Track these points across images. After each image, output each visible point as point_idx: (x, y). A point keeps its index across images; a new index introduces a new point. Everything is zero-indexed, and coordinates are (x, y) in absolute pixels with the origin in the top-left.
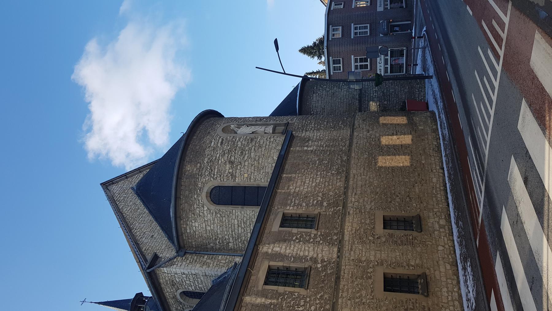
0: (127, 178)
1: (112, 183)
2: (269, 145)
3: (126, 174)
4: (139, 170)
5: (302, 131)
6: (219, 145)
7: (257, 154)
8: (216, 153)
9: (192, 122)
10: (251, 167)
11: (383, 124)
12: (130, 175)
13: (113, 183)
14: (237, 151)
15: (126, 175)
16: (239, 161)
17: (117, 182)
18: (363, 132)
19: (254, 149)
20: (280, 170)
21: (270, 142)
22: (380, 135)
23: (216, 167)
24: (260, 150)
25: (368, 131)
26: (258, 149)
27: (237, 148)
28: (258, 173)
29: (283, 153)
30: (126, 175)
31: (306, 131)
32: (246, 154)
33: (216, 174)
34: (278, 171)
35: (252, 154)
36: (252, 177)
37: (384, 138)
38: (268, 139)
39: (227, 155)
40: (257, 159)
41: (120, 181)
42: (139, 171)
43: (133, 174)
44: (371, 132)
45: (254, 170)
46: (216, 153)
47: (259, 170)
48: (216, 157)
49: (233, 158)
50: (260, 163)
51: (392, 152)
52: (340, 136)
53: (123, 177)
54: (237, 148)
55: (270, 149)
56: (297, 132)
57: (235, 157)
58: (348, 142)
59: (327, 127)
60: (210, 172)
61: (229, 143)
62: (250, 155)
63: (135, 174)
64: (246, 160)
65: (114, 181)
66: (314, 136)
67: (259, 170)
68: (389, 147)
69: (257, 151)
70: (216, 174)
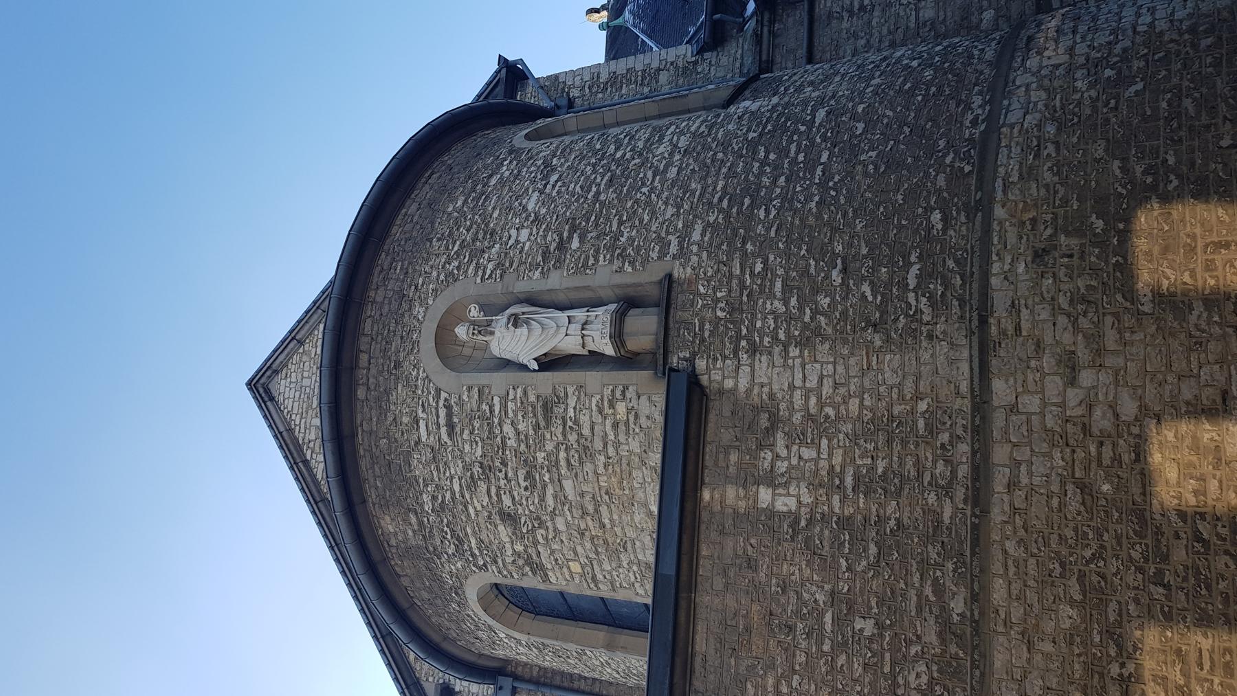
0: (301, 343)
1: (273, 373)
2: (617, 444)
3: (293, 335)
4: (318, 308)
5: (736, 352)
6: (445, 437)
7: (585, 489)
8: (448, 474)
9: (349, 234)
10: (582, 539)
11: (1163, 299)
12: (302, 332)
13: (276, 372)
14: (512, 468)
15: (295, 336)
16: (531, 512)
17: (285, 365)
18: (1043, 376)
19: (568, 461)
20: (675, 681)
21: (615, 425)
22: (1144, 411)
23: (469, 530)
24: (588, 467)
25: (1070, 369)
26: (581, 463)
27: (508, 452)
28: (614, 565)
29: (670, 570)
30: (293, 338)
31: (754, 350)
32: (544, 486)
33: (477, 552)
34: (667, 686)
35: (568, 485)
36: (599, 576)
37: (1170, 436)
38: (607, 411)
39: (483, 487)
40: (591, 509)
41: (289, 360)
42: (320, 311)
43: (311, 326)
44: (1086, 378)
45: (597, 553)
46: (448, 474)
47: (614, 554)
48: (453, 492)
49: (507, 501)
50: (608, 526)
51: (1222, 585)
52: (918, 396)
53: (291, 345)
54: (508, 452)
55: (624, 461)
56: (715, 359)
57: (513, 498)
58: (964, 448)
59: (844, 314)
60: (457, 547)
61: (473, 429)
62: (562, 488)
63: (314, 323)
64: (554, 509)
65: (274, 366)
66: (792, 387)
67: (614, 554)
68: (1205, 529)
69: (580, 475)
70: (477, 552)
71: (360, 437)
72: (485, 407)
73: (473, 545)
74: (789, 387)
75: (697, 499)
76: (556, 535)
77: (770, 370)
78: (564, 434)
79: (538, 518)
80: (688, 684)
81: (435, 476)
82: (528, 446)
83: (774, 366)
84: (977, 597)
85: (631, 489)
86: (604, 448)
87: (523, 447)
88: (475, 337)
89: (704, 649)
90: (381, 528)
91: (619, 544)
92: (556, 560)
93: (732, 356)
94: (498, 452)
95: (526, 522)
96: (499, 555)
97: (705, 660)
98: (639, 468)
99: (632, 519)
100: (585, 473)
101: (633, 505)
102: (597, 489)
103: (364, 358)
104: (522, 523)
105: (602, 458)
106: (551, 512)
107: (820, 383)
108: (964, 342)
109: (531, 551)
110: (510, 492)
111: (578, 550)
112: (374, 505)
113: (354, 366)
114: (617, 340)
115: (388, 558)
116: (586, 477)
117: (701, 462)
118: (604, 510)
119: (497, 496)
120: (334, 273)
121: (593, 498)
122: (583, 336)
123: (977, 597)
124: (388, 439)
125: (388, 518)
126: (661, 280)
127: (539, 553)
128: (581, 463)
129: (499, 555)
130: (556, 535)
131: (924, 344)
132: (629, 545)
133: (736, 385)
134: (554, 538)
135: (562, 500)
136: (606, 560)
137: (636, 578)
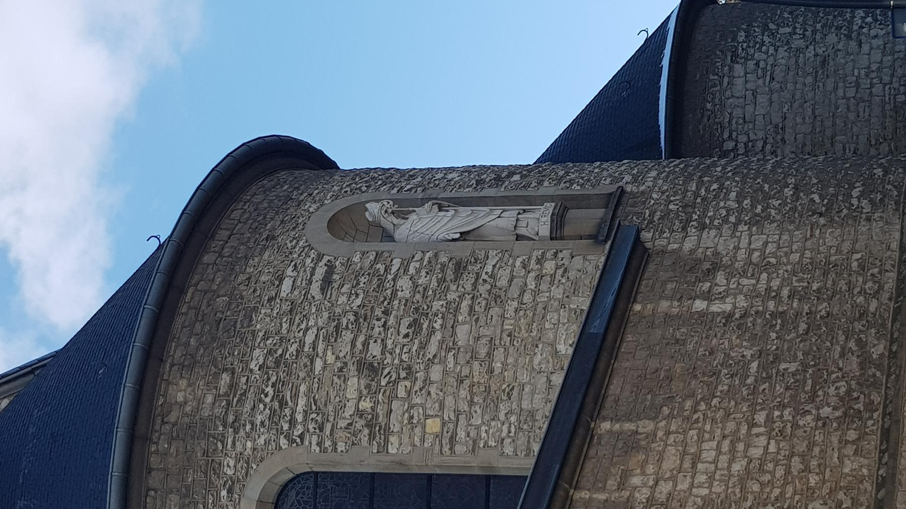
2: (537, 292)
7: (484, 331)
24: (495, 311)
26: (488, 308)
29: (597, 326)
33: (299, 418)
34: (578, 405)
36: (461, 434)
38: (533, 264)
39: (348, 336)
40: (483, 352)
45: (471, 403)
47: (492, 403)
48: (302, 344)
49: (375, 349)
56: (662, 232)
60: (273, 412)
64: (435, 356)
67: (492, 403)
70: (299, 418)
71: (189, 295)
72: (381, 267)
73: (300, 408)
74: (734, 248)
75: (627, 310)
76: (423, 387)
77: (717, 239)
78: (475, 285)
79: (409, 368)
80: (586, 446)
81: (284, 328)
82: (424, 296)
83: (721, 236)
84: (900, 373)
85: (540, 331)
86: (520, 296)
87: (418, 297)
88: (386, 216)
89: (618, 392)
90: (165, 396)
91: (504, 391)
92: (411, 417)
93: (680, 230)
94: (383, 302)
95: (389, 373)
96: (331, 419)
97: (616, 401)
98: (557, 311)
99: (531, 361)
100: (489, 317)
101: (537, 346)
102: (499, 331)
103: (223, 234)
104: (384, 374)
105: (515, 304)
106: (429, 359)
107: (764, 246)
108: (897, 221)
109: (381, 410)
110: (383, 340)
111: (447, 403)
112: (172, 365)
113: (210, 236)
114: (559, 219)
115: (151, 440)
116: (489, 321)
117: (636, 286)
118: (499, 354)
119: (363, 345)
120: (169, 234)
121: (491, 341)
122: (517, 220)
123: (900, 373)
124: (230, 298)
125: (183, 383)
126: (611, 194)
127: (391, 411)
128: (488, 308)
129: (331, 419)
130: (423, 387)
131: (863, 223)
132: (515, 393)
133: (681, 248)
134: (421, 390)
135: (449, 346)
136: (479, 411)
137: (510, 432)
